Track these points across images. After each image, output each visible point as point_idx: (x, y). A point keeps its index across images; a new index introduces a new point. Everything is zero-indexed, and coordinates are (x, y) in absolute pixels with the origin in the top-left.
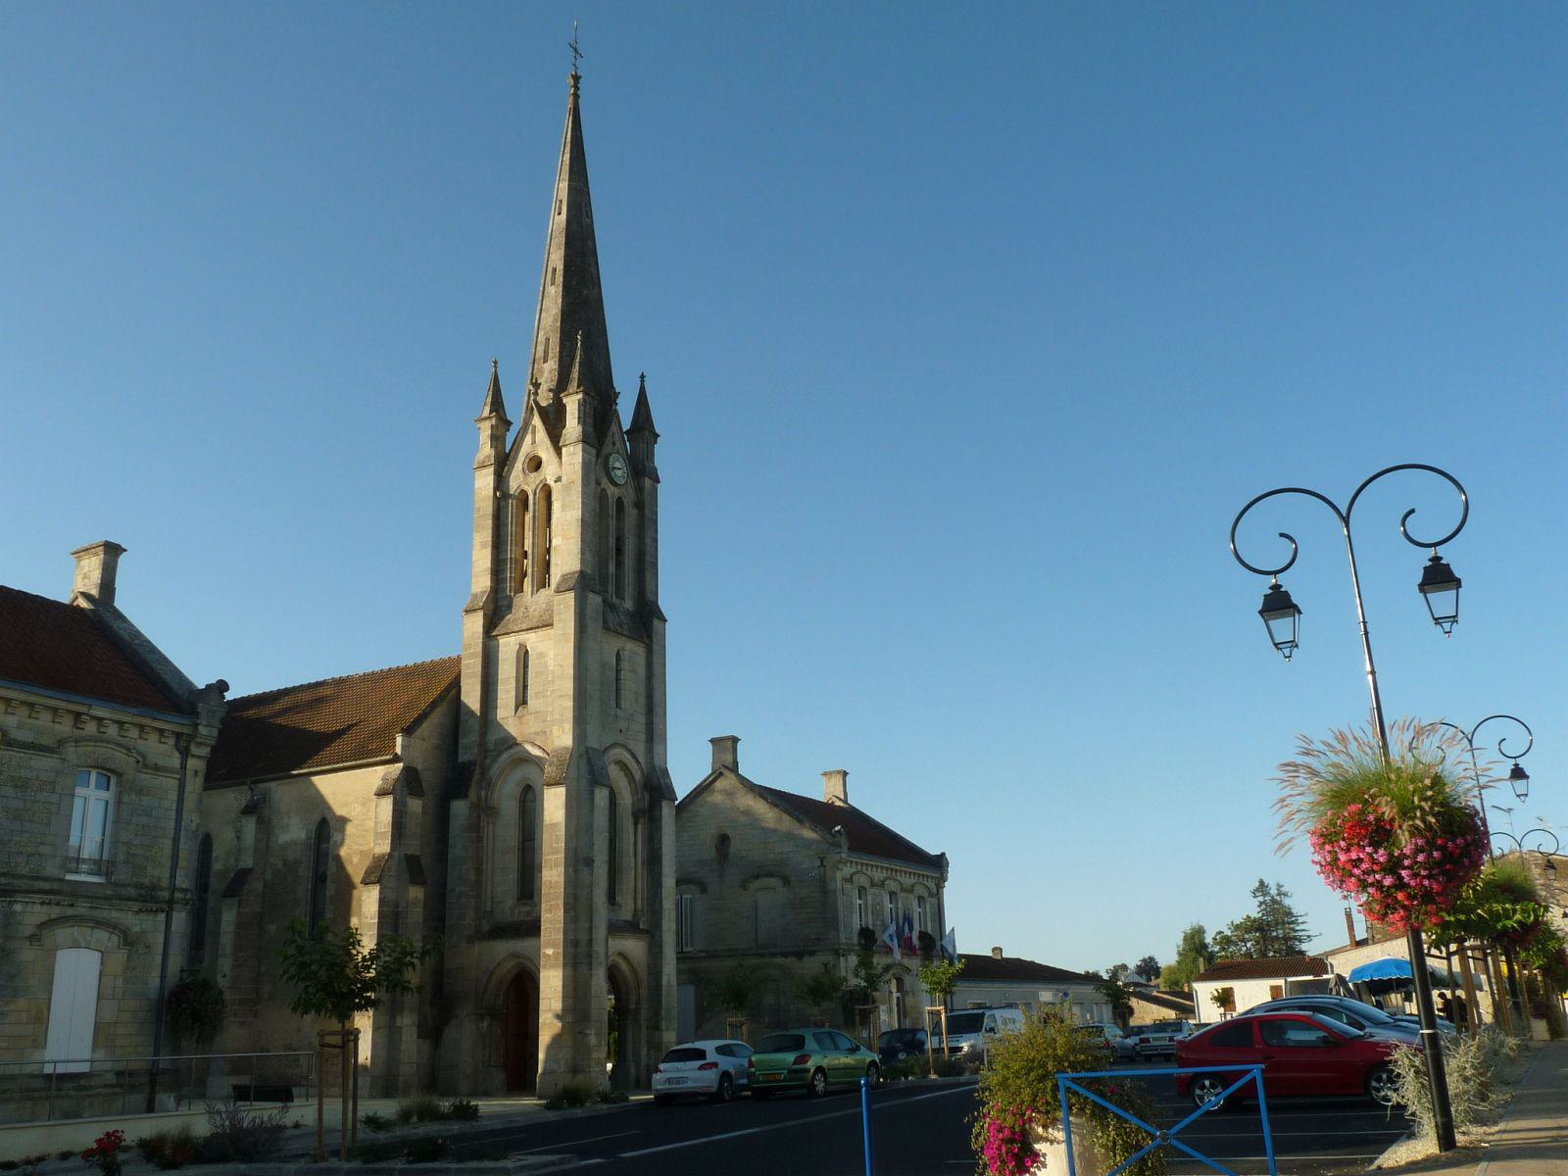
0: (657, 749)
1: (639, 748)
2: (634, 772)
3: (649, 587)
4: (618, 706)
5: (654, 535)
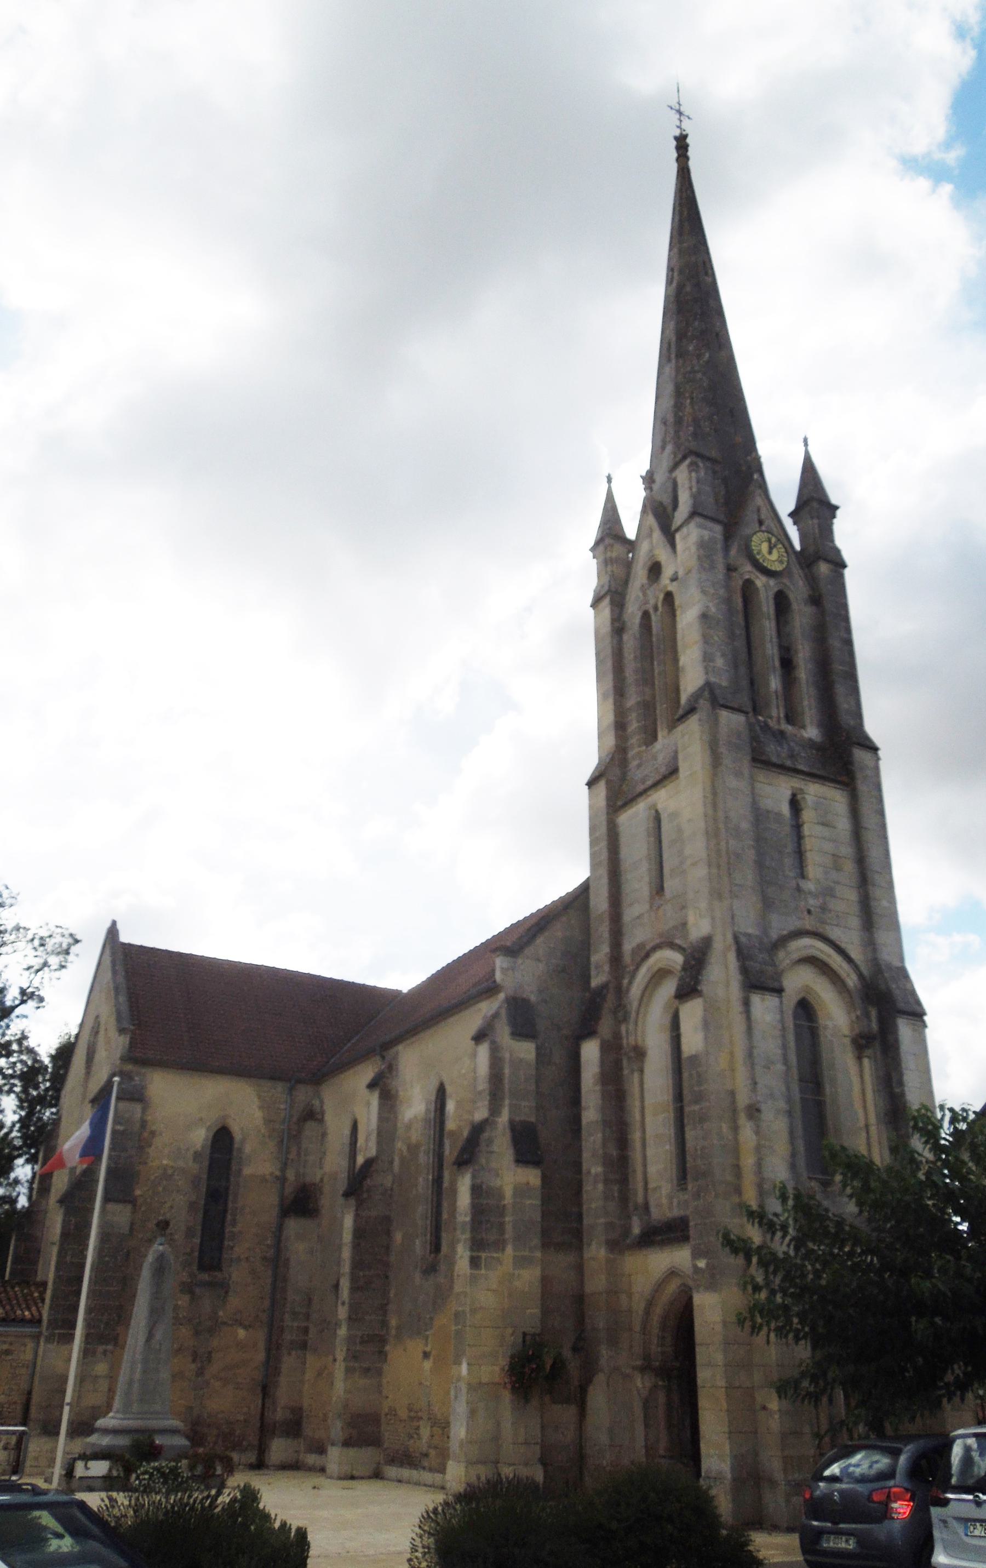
0: (882, 937)
1: (851, 938)
2: (843, 974)
3: (843, 704)
4: (803, 876)
5: (845, 636)
